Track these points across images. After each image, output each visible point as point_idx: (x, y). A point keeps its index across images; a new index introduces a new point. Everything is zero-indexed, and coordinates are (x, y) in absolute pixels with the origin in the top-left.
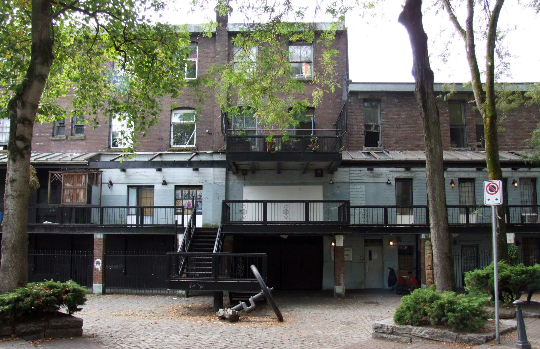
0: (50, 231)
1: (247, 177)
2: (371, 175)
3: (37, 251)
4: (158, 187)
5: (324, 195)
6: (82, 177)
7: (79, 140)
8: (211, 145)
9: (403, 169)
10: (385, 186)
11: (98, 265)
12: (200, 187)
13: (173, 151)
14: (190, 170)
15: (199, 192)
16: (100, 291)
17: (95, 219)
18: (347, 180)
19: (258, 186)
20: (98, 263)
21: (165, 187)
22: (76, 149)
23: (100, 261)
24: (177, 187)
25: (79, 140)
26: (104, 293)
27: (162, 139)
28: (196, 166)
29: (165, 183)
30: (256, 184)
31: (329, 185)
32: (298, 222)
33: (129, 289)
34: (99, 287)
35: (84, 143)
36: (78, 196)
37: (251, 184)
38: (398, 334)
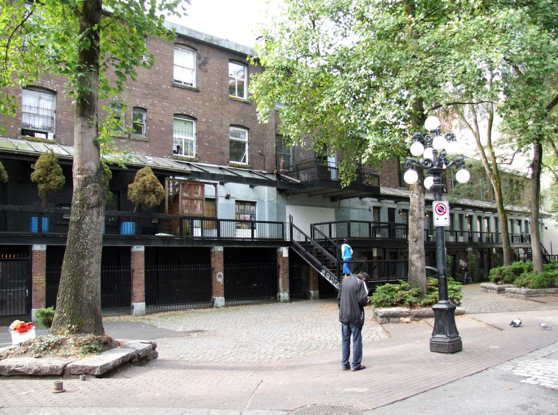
0: (168, 244)
1: (289, 197)
2: (361, 203)
3: (157, 267)
4: (221, 201)
5: (336, 217)
6: (198, 188)
7: (143, 141)
8: (263, 165)
9: (393, 202)
10: (368, 212)
11: (219, 278)
12: (253, 204)
13: (234, 166)
14: (247, 186)
15: (252, 208)
16: (223, 303)
17: (129, 230)
18: (348, 206)
19: (296, 207)
20: (220, 276)
21: (227, 201)
22: (139, 151)
23: (222, 274)
24: (237, 201)
25: (143, 141)
26: (226, 306)
27: (223, 153)
28: (253, 183)
29: (228, 197)
30: (295, 204)
31: (339, 208)
32: (230, 238)
33: (205, 303)
34: (222, 300)
35: (148, 145)
36: (196, 207)
37: (292, 204)
38: (538, 293)
